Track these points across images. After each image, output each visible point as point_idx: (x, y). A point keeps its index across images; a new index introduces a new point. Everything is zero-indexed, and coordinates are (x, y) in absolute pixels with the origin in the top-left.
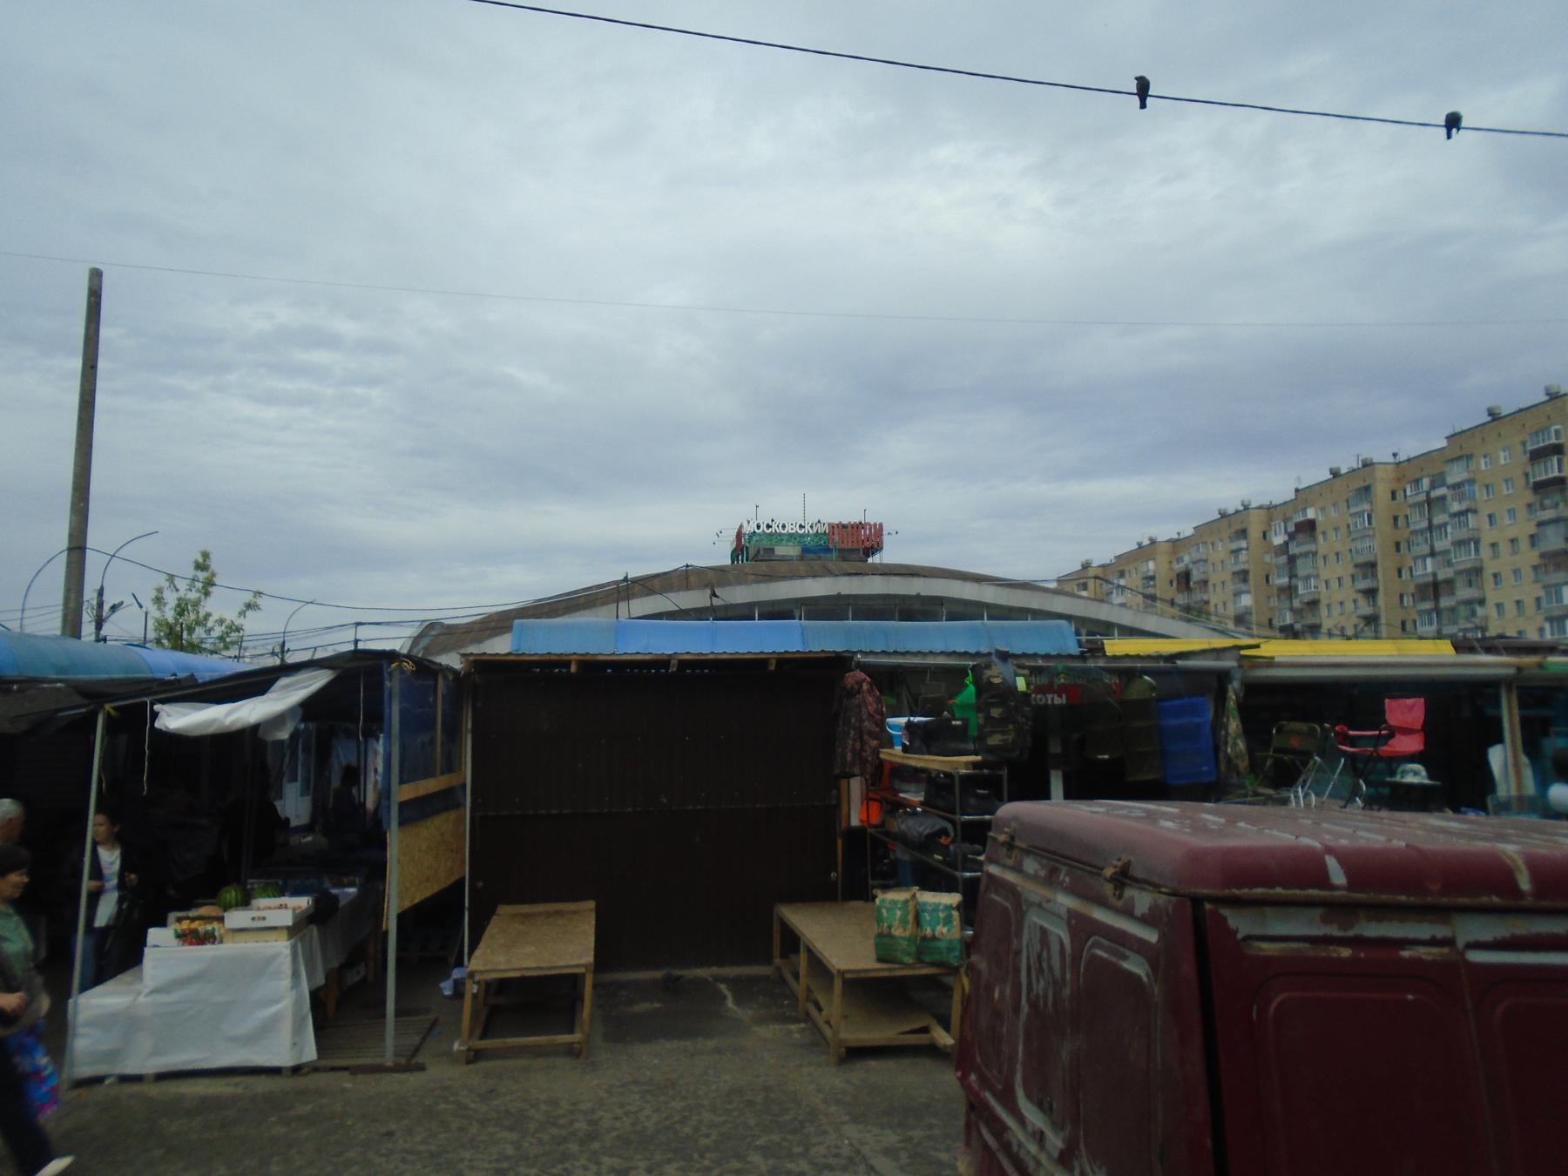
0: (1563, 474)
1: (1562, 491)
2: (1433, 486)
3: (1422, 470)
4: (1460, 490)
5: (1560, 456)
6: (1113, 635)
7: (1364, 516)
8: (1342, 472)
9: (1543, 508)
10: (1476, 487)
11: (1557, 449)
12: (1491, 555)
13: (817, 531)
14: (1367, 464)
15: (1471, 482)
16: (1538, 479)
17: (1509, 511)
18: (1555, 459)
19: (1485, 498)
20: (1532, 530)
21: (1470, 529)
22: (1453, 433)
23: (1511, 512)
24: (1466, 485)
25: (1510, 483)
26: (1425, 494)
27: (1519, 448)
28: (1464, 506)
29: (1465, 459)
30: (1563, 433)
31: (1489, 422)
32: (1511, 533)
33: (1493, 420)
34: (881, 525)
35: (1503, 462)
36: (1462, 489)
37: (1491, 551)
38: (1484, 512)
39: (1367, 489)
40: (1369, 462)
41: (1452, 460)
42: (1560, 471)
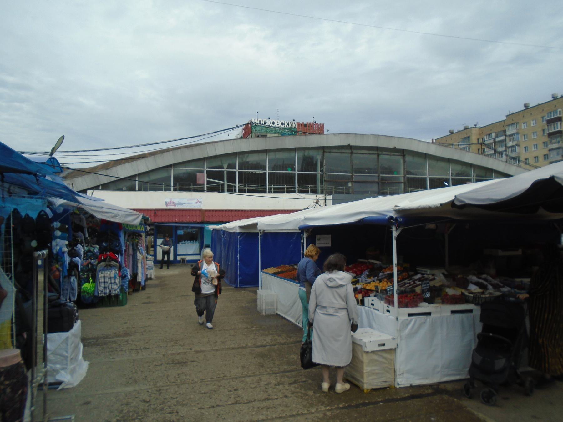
0: (561, 129)
1: (561, 136)
2: (497, 136)
3: (491, 130)
4: (513, 137)
5: (561, 122)
6: (492, 177)
7: (467, 149)
8: (454, 132)
9: (551, 143)
10: (520, 136)
11: (559, 119)
12: (534, 162)
13: (291, 127)
14: (466, 128)
15: (518, 133)
16: (550, 131)
17: (534, 145)
18: (559, 123)
19: (524, 140)
20: (546, 152)
21: (517, 153)
22: (509, 114)
23: (536, 146)
24: (516, 135)
25: (535, 134)
26: (493, 140)
27: (541, 120)
28: (514, 143)
29: (467, 138)
30: (562, 112)
31: (552, 100)
32: (535, 154)
33: (526, 109)
34: (323, 125)
35: (532, 125)
36: (514, 137)
37: (534, 160)
38: (523, 146)
39: (469, 137)
40: (467, 128)
41: (509, 125)
42: (560, 128)
